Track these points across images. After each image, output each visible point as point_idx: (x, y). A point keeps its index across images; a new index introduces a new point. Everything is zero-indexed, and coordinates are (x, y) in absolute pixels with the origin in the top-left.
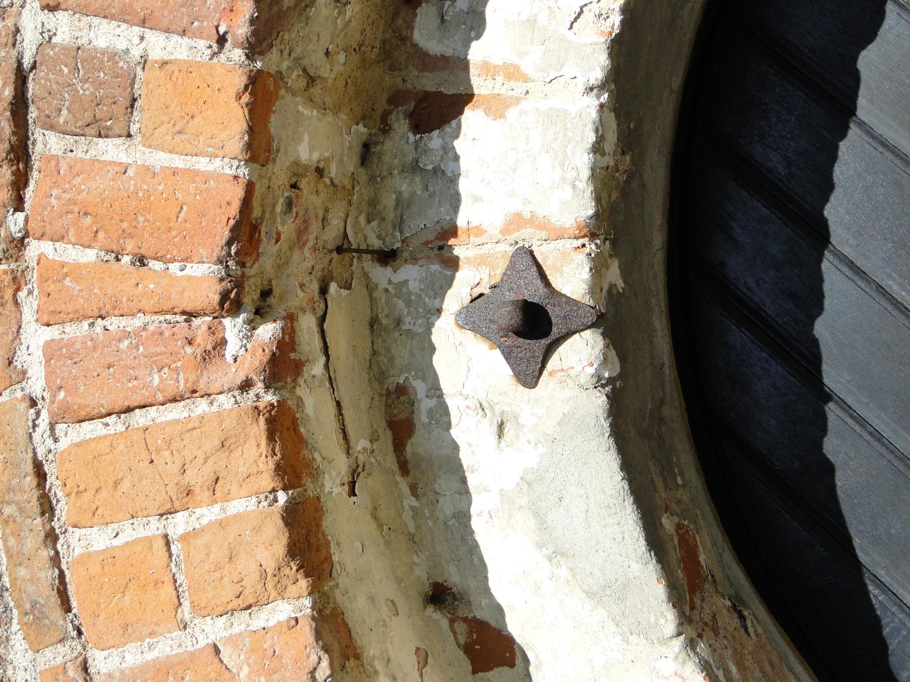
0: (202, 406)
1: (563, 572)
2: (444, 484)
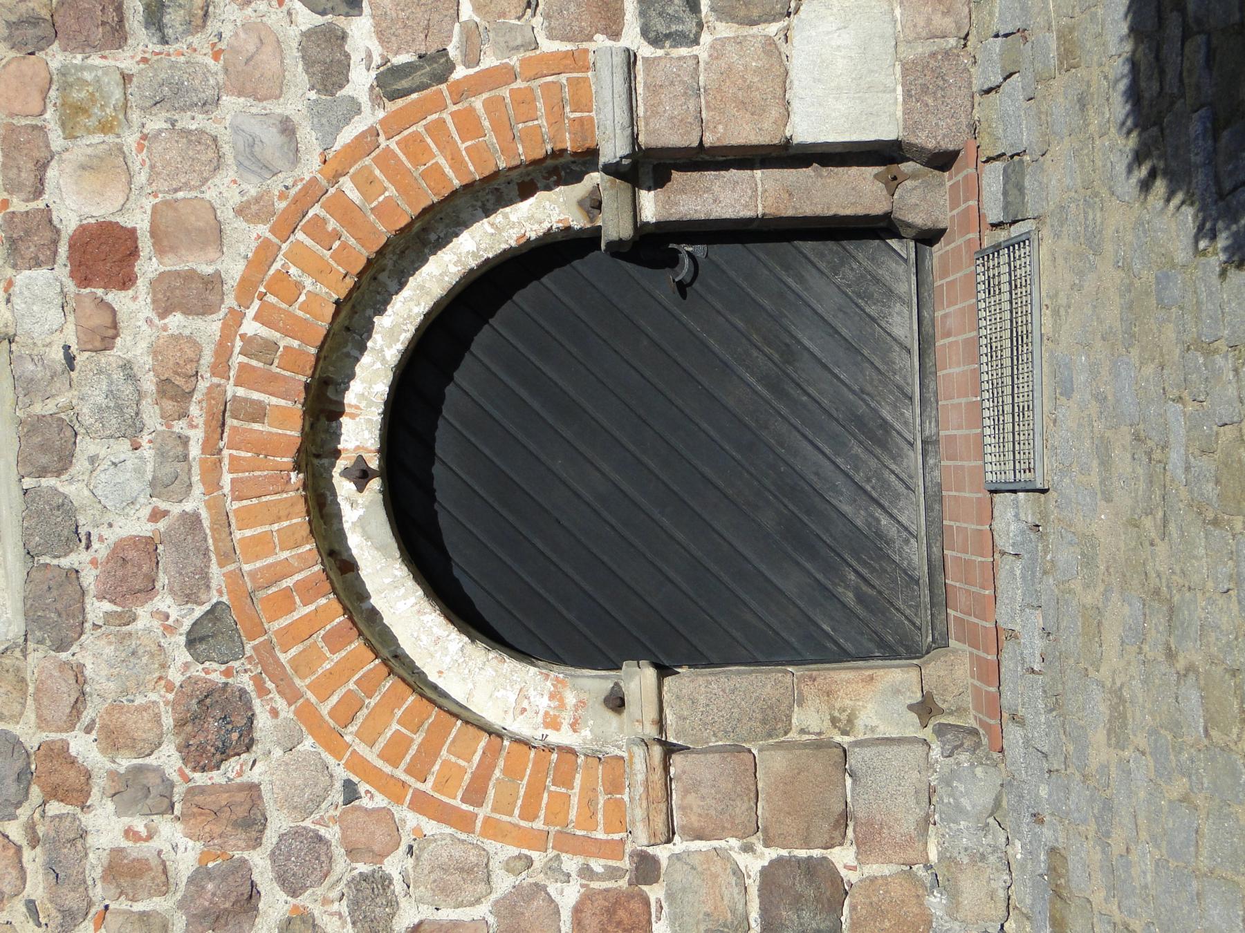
0: (285, 495)
1: (369, 543)
2: (335, 521)
